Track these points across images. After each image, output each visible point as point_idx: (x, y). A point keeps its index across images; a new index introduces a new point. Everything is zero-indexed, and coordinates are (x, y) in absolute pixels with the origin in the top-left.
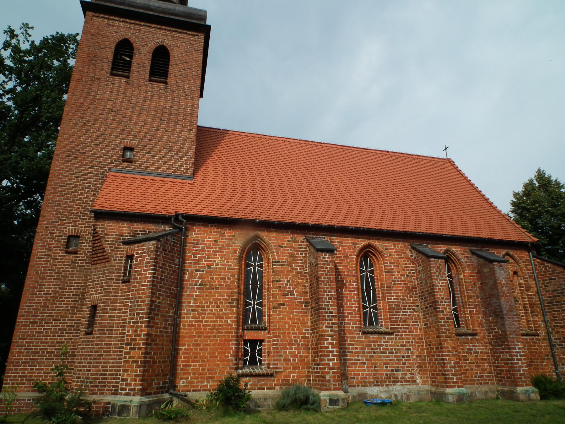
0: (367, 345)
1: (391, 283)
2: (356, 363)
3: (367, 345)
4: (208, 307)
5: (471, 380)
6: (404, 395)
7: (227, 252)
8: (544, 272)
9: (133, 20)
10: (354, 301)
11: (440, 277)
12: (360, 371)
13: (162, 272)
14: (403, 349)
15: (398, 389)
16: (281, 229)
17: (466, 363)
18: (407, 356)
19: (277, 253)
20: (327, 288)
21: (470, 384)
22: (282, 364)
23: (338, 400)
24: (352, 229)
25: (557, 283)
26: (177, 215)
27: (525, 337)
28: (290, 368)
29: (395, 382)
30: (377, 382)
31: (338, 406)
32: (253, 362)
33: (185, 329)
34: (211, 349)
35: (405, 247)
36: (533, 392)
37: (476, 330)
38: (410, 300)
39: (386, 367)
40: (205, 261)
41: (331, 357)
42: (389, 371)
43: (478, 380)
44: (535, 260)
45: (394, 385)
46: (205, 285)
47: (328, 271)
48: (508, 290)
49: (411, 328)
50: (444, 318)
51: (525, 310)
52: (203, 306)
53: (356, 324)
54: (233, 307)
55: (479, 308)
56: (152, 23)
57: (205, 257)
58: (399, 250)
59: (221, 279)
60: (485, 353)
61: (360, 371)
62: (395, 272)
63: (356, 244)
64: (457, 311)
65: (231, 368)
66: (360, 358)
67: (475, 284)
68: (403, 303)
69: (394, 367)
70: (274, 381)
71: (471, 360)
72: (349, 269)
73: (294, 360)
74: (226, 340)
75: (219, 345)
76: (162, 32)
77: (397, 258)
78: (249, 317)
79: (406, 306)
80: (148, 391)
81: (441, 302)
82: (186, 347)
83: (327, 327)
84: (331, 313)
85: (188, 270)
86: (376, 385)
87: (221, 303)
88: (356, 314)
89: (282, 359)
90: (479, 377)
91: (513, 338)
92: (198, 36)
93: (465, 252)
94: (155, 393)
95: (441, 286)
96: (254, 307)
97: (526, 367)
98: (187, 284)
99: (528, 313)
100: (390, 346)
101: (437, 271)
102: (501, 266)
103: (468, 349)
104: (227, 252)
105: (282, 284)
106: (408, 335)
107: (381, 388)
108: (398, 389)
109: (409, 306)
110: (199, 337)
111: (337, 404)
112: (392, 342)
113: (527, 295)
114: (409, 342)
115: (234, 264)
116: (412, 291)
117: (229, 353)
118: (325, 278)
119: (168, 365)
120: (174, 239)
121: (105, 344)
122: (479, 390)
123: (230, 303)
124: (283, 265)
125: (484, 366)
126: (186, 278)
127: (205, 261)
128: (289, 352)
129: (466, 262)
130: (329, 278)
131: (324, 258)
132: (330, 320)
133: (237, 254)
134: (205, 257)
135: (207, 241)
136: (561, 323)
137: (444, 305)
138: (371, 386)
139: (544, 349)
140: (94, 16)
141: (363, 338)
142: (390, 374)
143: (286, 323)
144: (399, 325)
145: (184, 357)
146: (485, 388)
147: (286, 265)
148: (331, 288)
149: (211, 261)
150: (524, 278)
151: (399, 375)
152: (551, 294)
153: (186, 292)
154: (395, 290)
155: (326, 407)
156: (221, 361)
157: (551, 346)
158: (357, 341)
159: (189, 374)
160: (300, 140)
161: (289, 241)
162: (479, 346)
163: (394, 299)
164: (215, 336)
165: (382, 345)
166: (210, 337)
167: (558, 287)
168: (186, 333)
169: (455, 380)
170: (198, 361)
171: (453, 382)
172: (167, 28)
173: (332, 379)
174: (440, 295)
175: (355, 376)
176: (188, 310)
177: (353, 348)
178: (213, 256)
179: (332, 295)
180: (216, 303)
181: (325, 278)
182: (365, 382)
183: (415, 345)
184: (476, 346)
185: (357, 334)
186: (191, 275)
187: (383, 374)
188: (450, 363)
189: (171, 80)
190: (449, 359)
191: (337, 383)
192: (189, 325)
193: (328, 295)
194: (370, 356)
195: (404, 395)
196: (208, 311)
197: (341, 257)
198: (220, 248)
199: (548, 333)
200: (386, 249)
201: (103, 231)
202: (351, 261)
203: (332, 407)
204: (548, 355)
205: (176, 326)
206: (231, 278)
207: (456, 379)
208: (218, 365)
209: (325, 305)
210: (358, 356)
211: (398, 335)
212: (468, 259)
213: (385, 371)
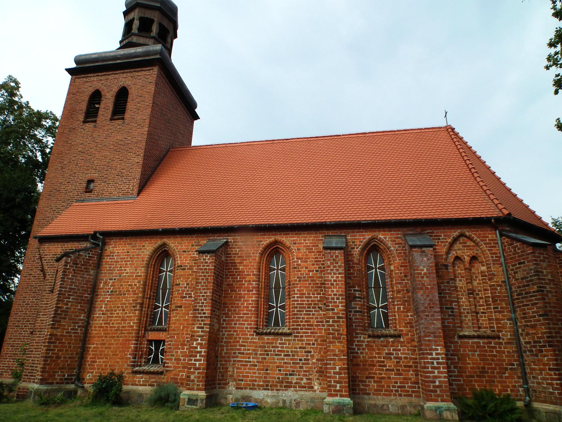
0: (260, 347)
1: (296, 280)
2: (247, 365)
3: (260, 347)
4: (115, 311)
5: (386, 391)
6: (293, 402)
7: (136, 261)
8: (514, 254)
9: (103, 72)
10: (252, 301)
11: (335, 271)
12: (250, 373)
13: (72, 282)
14: (301, 352)
15: (290, 395)
16: (201, 234)
17: (383, 370)
18: (305, 360)
19: (180, 258)
20: (204, 289)
21: (384, 395)
22: (173, 364)
23: (197, 400)
24: (253, 227)
25: (526, 268)
26: (95, 233)
27: (476, 340)
28: (180, 367)
29: (288, 387)
30: (267, 386)
31: (196, 406)
32: (156, 361)
33: (95, 330)
34: (114, 348)
35: (317, 240)
36: (448, 409)
37: (402, 331)
38: (317, 297)
39: (280, 370)
40: (118, 270)
41: (198, 358)
42: (282, 374)
43: (397, 391)
44: (504, 239)
45: (286, 390)
46: (116, 292)
47: (207, 273)
48: (431, 281)
49: (314, 329)
50: (333, 318)
51: (487, 305)
52: (112, 310)
53: (251, 324)
54: (136, 310)
55: (409, 305)
56: (117, 70)
57: (117, 267)
58: (310, 243)
59: (129, 285)
60: (411, 358)
61: (250, 373)
62: (302, 268)
63: (261, 241)
64: (387, 309)
65: (128, 365)
66: (251, 360)
67: (406, 276)
68: (308, 301)
69: (289, 371)
70: (164, 378)
71: (389, 366)
72: (250, 269)
73: (184, 360)
74: (126, 340)
75: (120, 345)
76: (124, 75)
77: (306, 252)
78: (150, 318)
79: (311, 304)
80: (49, 381)
81: (333, 299)
82: (95, 346)
83: (198, 328)
84: (204, 313)
85: (103, 280)
86: (265, 389)
87: (126, 307)
89: (174, 358)
90: (399, 387)
91: (429, 341)
92: (152, 69)
93: (398, 238)
94: (57, 383)
95: (335, 281)
96: (277, 310)
97: (445, 377)
98: (101, 292)
99: (491, 308)
100: (286, 348)
101: (332, 263)
102: (424, 252)
103: (387, 354)
104: (136, 261)
105: (181, 287)
106: (310, 336)
107: (270, 393)
108: (290, 395)
109: (315, 304)
110: (106, 337)
111: (195, 404)
112: (289, 344)
113: (491, 286)
114: (309, 344)
115: (141, 271)
116: (321, 287)
117: (128, 351)
118: (203, 279)
119: (77, 361)
120: (89, 254)
121: (36, 343)
122: (394, 402)
123: (134, 307)
124: (185, 269)
125: (408, 375)
126: (101, 286)
127: (118, 270)
128: (181, 352)
129: (397, 250)
131: (204, 259)
132: (202, 321)
133: (145, 262)
134: (117, 267)
135: (121, 253)
136: (531, 321)
137: (336, 302)
138: (259, 389)
139: (506, 356)
140: (76, 78)
141: (256, 339)
142: (282, 378)
143: (181, 324)
144: (300, 325)
145: (93, 355)
146: (404, 400)
147: (188, 269)
148: (208, 289)
149: (122, 270)
150: (487, 264)
151: (294, 379)
152: (521, 283)
153: (100, 298)
154: (300, 287)
155: (185, 407)
156: (121, 359)
157: (520, 351)
158: (250, 342)
159: (95, 369)
160: (425, 129)
161: (192, 246)
162: (404, 350)
163: (297, 297)
164: (118, 337)
165: (278, 347)
166: (114, 337)
167: (528, 274)
168: (96, 334)
169: (338, 388)
170: (102, 358)
171: (335, 391)
172: (128, 71)
173: (196, 379)
174: (333, 291)
175: (244, 379)
176: (100, 314)
178: (127, 264)
179: (207, 296)
180: (122, 307)
181: (203, 279)
182: (254, 385)
183: (317, 348)
184: (400, 350)
185: (250, 335)
187: (275, 378)
188: (335, 368)
189: (127, 116)
190: (334, 364)
191: (201, 384)
192: (99, 327)
193: (203, 296)
194: (262, 358)
195: (293, 402)
196: (116, 314)
197: (243, 257)
198: (131, 258)
199: (516, 335)
200: (295, 244)
201: (44, 253)
202: (253, 260)
203: (190, 406)
204: (513, 365)
205: (87, 326)
206: (138, 284)
207: (340, 387)
208: (118, 362)
209: (200, 306)
210: (249, 358)
211: (298, 336)
212: (399, 247)
213: (277, 374)
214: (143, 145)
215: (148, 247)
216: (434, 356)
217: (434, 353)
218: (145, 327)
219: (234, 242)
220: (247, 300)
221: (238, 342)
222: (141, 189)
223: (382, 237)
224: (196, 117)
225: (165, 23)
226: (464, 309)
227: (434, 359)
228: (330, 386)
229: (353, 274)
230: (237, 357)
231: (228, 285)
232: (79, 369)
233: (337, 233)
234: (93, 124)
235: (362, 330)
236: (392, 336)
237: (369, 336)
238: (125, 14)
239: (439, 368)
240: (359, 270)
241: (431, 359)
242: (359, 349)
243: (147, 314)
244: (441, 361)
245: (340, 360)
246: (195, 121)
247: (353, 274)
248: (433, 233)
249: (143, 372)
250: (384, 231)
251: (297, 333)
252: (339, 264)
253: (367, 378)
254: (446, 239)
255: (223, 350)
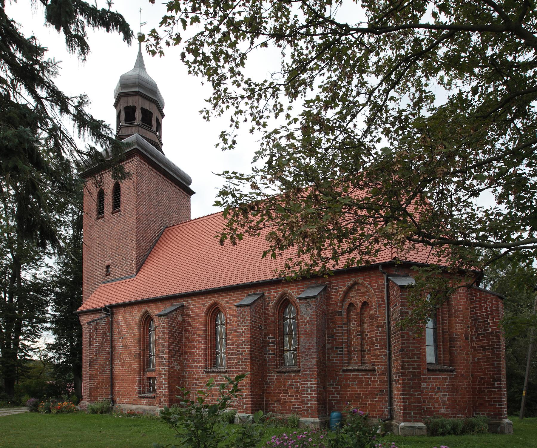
5: (288, 410)
11: (243, 324)
17: (286, 396)
41: (164, 388)
47: (164, 331)
53: (201, 366)
63: (205, 303)
71: (291, 393)
81: (242, 345)
83: (162, 368)
84: (165, 359)
88: (202, 359)
90: (296, 408)
91: (307, 374)
95: (243, 332)
101: (241, 318)
103: (289, 385)
115: (136, 332)
130: (164, 335)
137: (244, 348)
144: (232, 366)
148: (165, 342)
154: (232, 338)
165: (219, 381)
171: (243, 409)
177: (199, 383)
181: (162, 336)
184: (299, 382)
186: (118, 341)
189: (122, 208)
200: (228, 303)
205: (112, 368)
206: (135, 340)
211: (230, 373)
214: (134, 232)
215: (137, 314)
216: (309, 385)
217: (309, 383)
218: (144, 369)
219: (188, 305)
220: (199, 348)
221: (195, 378)
222: (139, 269)
223: (291, 291)
224: (192, 193)
225: (147, 106)
226: (354, 348)
227: (309, 387)
228: (240, 406)
229: (268, 324)
230: (195, 388)
231: (186, 338)
232: (112, 395)
233: (257, 291)
234: (103, 219)
235: (274, 368)
236: (293, 372)
237: (277, 372)
238: (116, 105)
239: (311, 394)
240: (274, 322)
241: (307, 388)
242: (271, 382)
243: (144, 361)
244: (313, 389)
245: (247, 389)
246: (191, 196)
247: (268, 324)
248: (331, 283)
249: (147, 398)
250: (293, 286)
251: (231, 371)
252: (247, 318)
253: (275, 401)
254: (341, 288)
255: (186, 383)
